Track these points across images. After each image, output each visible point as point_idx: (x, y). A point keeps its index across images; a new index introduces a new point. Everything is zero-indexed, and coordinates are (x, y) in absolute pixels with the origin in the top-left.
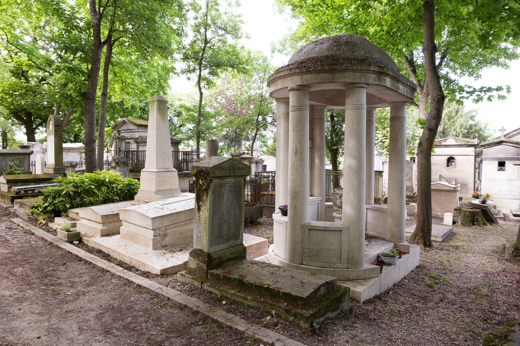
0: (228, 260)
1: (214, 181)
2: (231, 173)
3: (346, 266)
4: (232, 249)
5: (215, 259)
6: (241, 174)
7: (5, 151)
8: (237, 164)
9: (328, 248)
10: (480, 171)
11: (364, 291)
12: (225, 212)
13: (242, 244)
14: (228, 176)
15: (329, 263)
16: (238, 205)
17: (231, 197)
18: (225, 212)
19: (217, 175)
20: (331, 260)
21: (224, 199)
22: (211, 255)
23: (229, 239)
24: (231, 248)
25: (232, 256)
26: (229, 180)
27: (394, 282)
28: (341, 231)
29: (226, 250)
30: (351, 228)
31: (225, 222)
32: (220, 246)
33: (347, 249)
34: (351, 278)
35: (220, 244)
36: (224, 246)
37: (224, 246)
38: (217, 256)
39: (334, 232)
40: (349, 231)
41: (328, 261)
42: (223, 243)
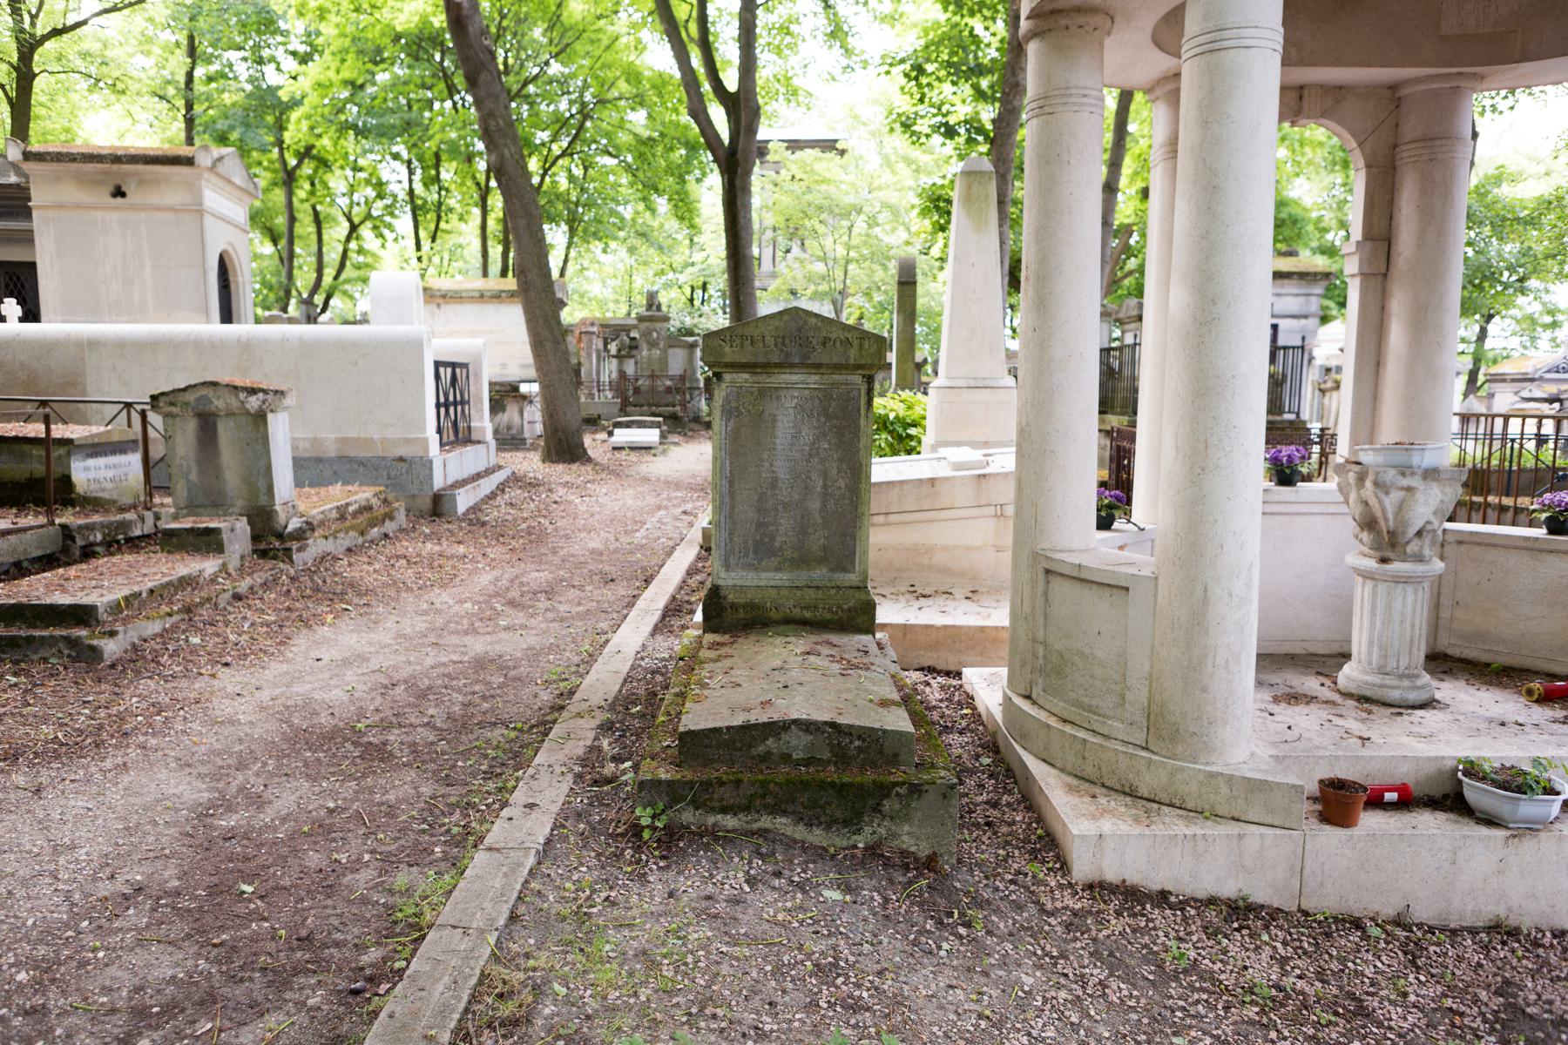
1: (727, 377)
3: (1140, 738)
4: (810, 595)
6: (835, 360)
8: (817, 329)
9: (1087, 651)
10: (229, 188)
11: (1102, 838)
12: (782, 471)
14: (781, 365)
15: (1090, 709)
16: (840, 460)
17: (807, 434)
18: (782, 471)
20: (1094, 702)
22: (722, 593)
23: (802, 560)
24: (811, 591)
25: (808, 615)
26: (795, 378)
27: (1502, 912)
28: (1127, 589)
29: (786, 592)
30: (1161, 582)
31: (786, 506)
32: (764, 575)
33: (1147, 667)
34: (1144, 792)
35: (766, 570)
36: (781, 578)
37: (781, 578)
38: (742, 601)
39: (1108, 590)
40: (1155, 596)
41: (1086, 700)
42: (778, 569)
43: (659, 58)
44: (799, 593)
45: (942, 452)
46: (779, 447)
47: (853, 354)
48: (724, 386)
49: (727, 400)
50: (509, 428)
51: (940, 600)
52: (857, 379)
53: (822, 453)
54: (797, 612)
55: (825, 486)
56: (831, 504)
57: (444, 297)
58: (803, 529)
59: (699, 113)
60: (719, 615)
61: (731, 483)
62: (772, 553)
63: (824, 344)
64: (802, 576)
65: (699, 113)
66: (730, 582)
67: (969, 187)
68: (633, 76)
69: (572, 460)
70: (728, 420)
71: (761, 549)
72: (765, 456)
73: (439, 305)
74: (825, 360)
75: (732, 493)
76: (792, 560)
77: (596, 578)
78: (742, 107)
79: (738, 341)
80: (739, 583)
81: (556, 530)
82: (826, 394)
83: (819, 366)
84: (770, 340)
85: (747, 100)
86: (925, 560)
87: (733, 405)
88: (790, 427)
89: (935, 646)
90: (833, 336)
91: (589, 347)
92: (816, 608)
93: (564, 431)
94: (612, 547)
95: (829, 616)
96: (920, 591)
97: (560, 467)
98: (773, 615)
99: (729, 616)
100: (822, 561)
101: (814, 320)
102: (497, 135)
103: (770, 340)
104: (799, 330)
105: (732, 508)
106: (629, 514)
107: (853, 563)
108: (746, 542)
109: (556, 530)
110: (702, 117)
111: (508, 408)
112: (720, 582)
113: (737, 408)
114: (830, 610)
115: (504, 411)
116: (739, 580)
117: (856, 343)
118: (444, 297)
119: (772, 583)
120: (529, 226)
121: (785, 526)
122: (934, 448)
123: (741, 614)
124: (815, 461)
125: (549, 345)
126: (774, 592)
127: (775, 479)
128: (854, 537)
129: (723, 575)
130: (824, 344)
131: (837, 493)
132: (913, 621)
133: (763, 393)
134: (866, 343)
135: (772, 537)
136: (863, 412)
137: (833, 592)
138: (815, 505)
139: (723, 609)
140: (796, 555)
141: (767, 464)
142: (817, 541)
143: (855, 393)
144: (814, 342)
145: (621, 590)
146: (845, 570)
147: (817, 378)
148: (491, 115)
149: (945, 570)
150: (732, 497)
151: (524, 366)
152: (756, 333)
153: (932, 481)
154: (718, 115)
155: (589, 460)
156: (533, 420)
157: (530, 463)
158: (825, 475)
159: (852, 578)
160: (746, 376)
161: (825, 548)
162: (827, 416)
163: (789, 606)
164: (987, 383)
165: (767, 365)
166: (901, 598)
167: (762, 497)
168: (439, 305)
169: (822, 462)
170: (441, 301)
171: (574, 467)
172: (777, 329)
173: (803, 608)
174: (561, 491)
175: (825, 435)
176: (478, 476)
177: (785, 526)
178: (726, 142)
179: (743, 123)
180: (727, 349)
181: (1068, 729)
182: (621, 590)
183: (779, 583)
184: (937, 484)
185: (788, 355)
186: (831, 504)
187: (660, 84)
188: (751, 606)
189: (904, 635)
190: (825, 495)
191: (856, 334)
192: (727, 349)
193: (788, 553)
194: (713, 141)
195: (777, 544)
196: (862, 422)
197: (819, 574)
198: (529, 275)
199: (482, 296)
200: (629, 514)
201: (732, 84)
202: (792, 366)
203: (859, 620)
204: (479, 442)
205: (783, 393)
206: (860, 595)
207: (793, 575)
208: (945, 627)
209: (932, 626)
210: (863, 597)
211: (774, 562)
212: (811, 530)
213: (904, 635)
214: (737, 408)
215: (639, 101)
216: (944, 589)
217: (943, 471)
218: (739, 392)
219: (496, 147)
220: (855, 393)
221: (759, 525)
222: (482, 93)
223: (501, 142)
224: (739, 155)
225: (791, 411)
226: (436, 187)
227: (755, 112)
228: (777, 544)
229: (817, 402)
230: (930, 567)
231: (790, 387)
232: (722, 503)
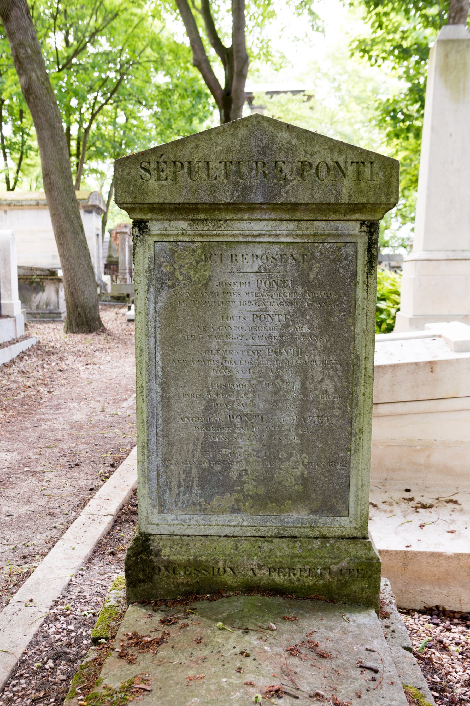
0: (250, 589)
2: (245, 190)
4: (283, 549)
5: (171, 567)
6: (319, 197)
7: (11, 196)
8: (290, 149)
12: (240, 369)
13: (361, 538)
14: (234, 207)
16: (327, 351)
17: (277, 313)
18: (240, 369)
19: (153, 199)
21: (234, 312)
22: (154, 545)
23: (272, 498)
24: (284, 543)
25: (279, 579)
26: (257, 227)
29: (246, 545)
31: (246, 418)
32: (215, 519)
36: (241, 523)
37: (241, 523)
38: (182, 558)
42: (236, 510)
43: (174, 29)
44: (266, 546)
45: (434, 328)
46: (235, 332)
47: (346, 187)
48: (150, 240)
49: (155, 261)
50: (47, 304)
51: (445, 512)
52: (353, 227)
53: (300, 342)
54: (263, 576)
55: (304, 389)
56: (313, 417)
57: (9, 205)
58: (271, 454)
59: (202, 64)
60: (149, 578)
61: (165, 386)
62: (226, 487)
63: (301, 173)
64: (271, 522)
65: (202, 64)
66: (165, 530)
67: (447, 56)
68: (155, 43)
69: (90, 330)
70: (158, 291)
71: (209, 480)
72: (214, 346)
73: (5, 212)
74: (303, 198)
75: (166, 401)
76: (255, 497)
77: (63, 461)
78: (236, 59)
79: (168, 171)
80: (178, 530)
81: (51, 400)
82: (304, 253)
83: (293, 207)
84: (217, 169)
85: (238, 51)
86: (422, 459)
87: (166, 269)
88: (250, 299)
89: (444, 580)
90: (316, 160)
91: (123, 244)
92: (291, 569)
93: (82, 307)
94: (94, 420)
95: (310, 581)
96: (418, 499)
97: (79, 337)
98: (228, 578)
99: (164, 581)
100: (301, 498)
101: (284, 136)
102: (25, 61)
103: (217, 169)
104: (263, 151)
105: (167, 421)
106: (124, 382)
107: (346, 501)
108: (188, 472)
109: (51, 400)
110: (204, 65)
111: (47, 288)
112: (151, 530)
113: (171, 275)
114: (311, 573)
115: (43, 291)
116: (179, 527)
117: (351, 170)
118: (9, 205)
119: (227, 531)
120: (52, 137)
121: (245, 448)
122: (418, 321)
123: (181, 577)
124: (288, 354)
125: (69, 236)
126: (229, 545)
127: (229, 380)
128: (347, 464)
129: (155, 518)
130: (301, 173)
131: (323, 399)
132: (415, 548)
133: (209, 251)
134: (367, 171)
135: (227, 465)
136: (361, 277)
137: (317, 544)
138: (288, 417)
139: (155, 570)
140: (261, 490)
141: (217, 358)
142: (292, 470)
143: (350, 249)
144: (286, 169)
145: (83, 479)
146: (333, 511)
147: (291, 226)
148: (21, 44)
149: (446, 471)
150: (166, 405)
151: (53, 256)
152: (196, 157)
153: (431, 365)
154: (219, 71)
155: (104, 330)
156: (56, 296)
157: (54, 333)
158: (304, 372)
159: (344, 524)
160: (184, 225)
161: (304, 481)
162: (306, 284)
163: (251, 566)
164: (460, 256)
165: (214, 207)
166: (396, 509)
167: (210, 406)
168: (5, 212)
169: (299, 353)
170: (7, 208)
171: (90, 337)
172: (229, 150)
173: (278, 569)
174: (70, 359)
175: (303, 314)
176: (11, 343)
177: (245, 448)
178: (223, 87)
179: (235, 69)
180: (152, 183)
181: (233, 233)
182: (83, 479)
183: (238, 531)
184: (437, 369)
185: (245, 190)
186: (313, 417)
187: (175, 51)
188: (196, 565)
189: (405, 564)
190: (304, 403)
191: (351, 157)
192: (152, 183)
193: (250, 488)
194: (212, 83)
195: (233, 475)
196: (360, 292)
197: (296, 518)
198: (53, 177)
199: (38, 204)
200: (124, 382)
201: (227, 43)
202: (252, 208)
203: (356, 587)
204: (8, 316)
205: (239, 250)
206: (356, 550)
207: (258, 519)
208: (458, 556)
209: (440, 555)
210: (361, 553)
211: (229, 500)
212: (283, 455)
213: (405, 564)
214: (171, 275)
215: (160, 63)
216: (447, 495)
217: (442, 353)
218: (174, 249)
219: (25, 71)
220: (350, 249)
221: (207, 447)
222: (14, 26)
223: (29, 66)
224: (233, 94)
225: (252, 278)
226: (21, 134)
227: (245, 61)
228: (233, 475)
229: (291, 263)
230: (428, 467)
231: (250, 241)
232: (151, 415)
